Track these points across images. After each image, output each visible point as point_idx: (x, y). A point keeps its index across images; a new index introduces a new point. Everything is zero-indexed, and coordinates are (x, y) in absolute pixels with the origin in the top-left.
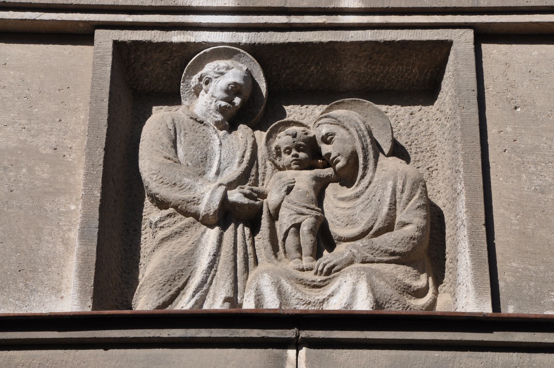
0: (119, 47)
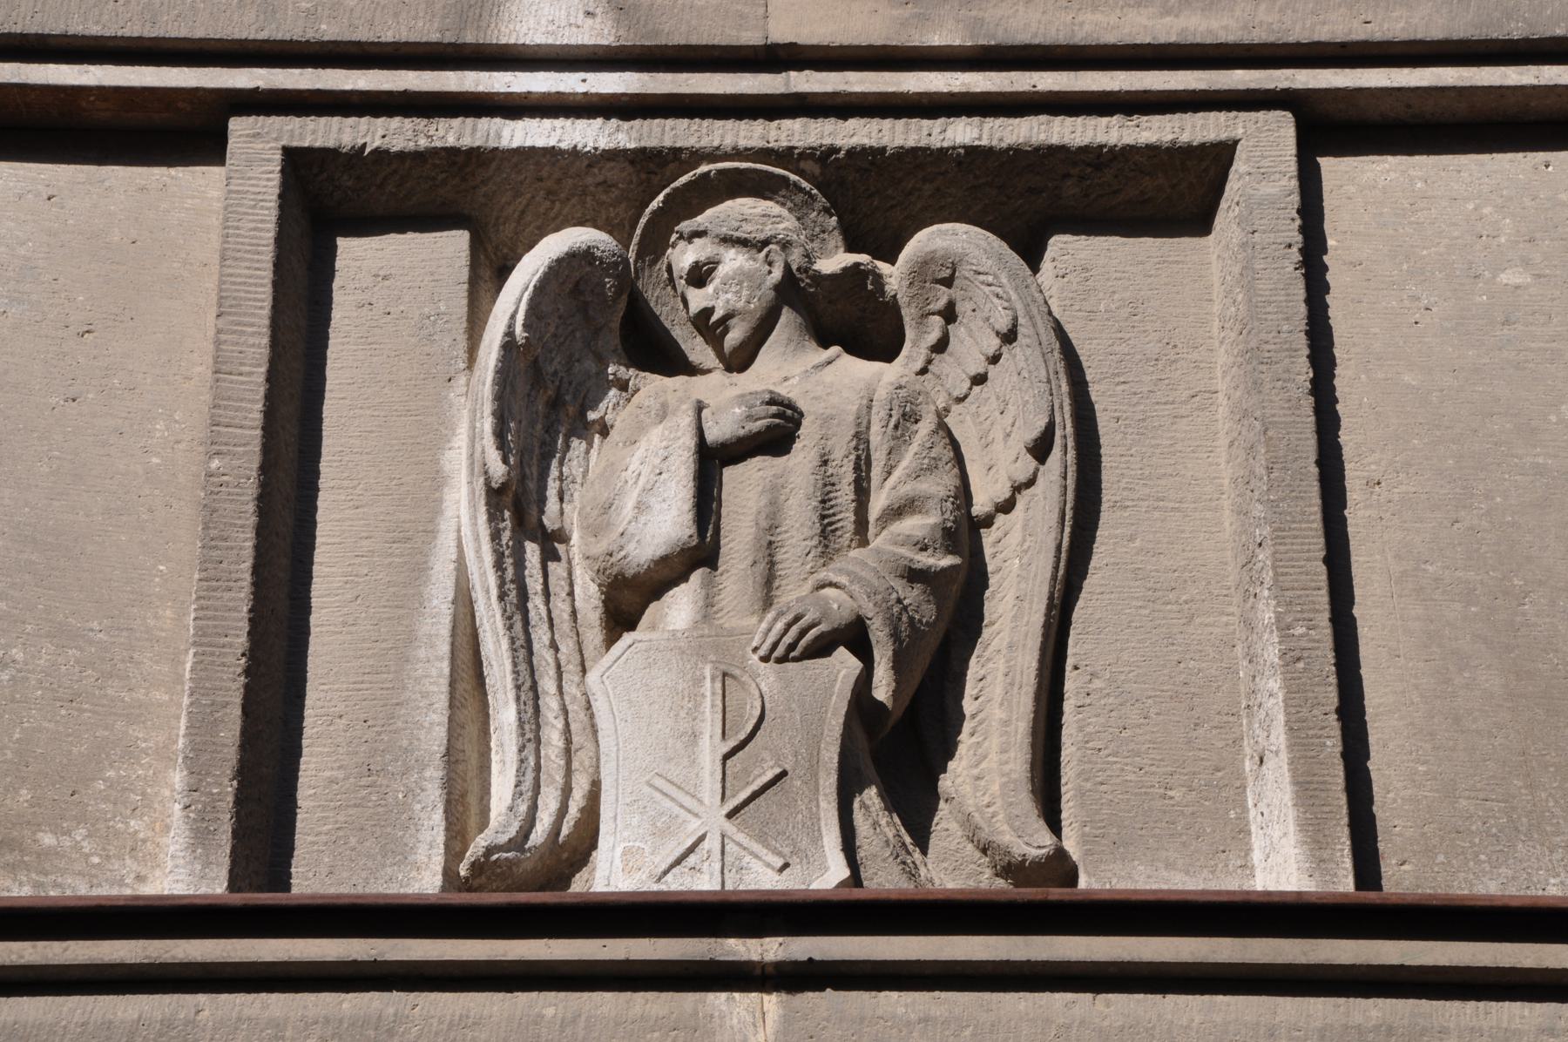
0: (297, 162)
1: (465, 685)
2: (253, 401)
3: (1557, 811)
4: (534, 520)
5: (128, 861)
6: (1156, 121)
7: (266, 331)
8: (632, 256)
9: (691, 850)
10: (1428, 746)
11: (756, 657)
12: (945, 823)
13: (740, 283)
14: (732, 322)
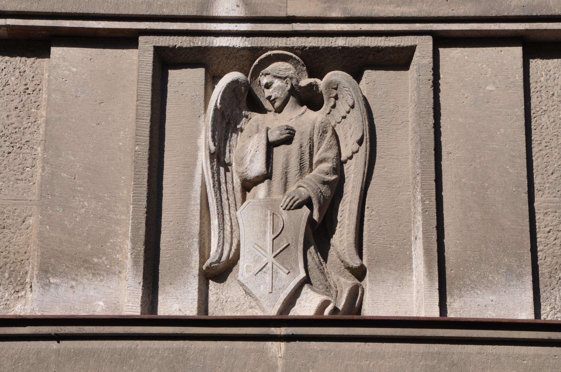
0: (158, 50)
1: (204, 211)
2: (147, 128)
3: (493, 254)
4: (222, 160)
5: (117, 267)
6: (395, 38)
7: (150, 105)
8: (249, 79)
9: (264, 267)
10: (460, 235)
11: (282, 208)
12: (332, 253)
13: (279, 90)
14: (277, 100)
